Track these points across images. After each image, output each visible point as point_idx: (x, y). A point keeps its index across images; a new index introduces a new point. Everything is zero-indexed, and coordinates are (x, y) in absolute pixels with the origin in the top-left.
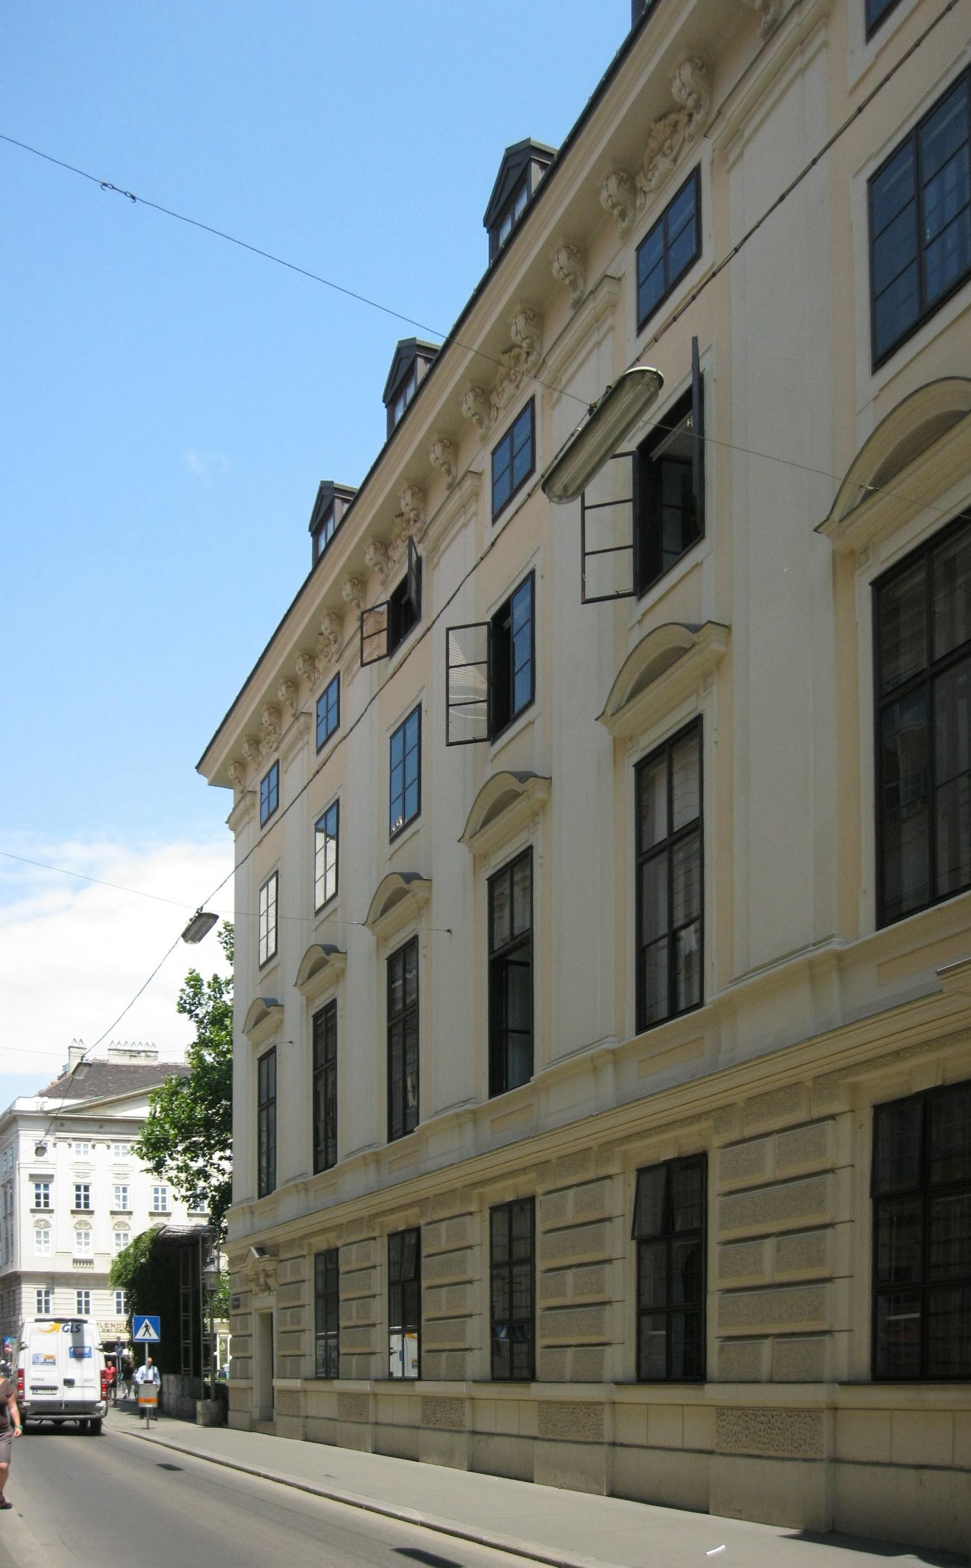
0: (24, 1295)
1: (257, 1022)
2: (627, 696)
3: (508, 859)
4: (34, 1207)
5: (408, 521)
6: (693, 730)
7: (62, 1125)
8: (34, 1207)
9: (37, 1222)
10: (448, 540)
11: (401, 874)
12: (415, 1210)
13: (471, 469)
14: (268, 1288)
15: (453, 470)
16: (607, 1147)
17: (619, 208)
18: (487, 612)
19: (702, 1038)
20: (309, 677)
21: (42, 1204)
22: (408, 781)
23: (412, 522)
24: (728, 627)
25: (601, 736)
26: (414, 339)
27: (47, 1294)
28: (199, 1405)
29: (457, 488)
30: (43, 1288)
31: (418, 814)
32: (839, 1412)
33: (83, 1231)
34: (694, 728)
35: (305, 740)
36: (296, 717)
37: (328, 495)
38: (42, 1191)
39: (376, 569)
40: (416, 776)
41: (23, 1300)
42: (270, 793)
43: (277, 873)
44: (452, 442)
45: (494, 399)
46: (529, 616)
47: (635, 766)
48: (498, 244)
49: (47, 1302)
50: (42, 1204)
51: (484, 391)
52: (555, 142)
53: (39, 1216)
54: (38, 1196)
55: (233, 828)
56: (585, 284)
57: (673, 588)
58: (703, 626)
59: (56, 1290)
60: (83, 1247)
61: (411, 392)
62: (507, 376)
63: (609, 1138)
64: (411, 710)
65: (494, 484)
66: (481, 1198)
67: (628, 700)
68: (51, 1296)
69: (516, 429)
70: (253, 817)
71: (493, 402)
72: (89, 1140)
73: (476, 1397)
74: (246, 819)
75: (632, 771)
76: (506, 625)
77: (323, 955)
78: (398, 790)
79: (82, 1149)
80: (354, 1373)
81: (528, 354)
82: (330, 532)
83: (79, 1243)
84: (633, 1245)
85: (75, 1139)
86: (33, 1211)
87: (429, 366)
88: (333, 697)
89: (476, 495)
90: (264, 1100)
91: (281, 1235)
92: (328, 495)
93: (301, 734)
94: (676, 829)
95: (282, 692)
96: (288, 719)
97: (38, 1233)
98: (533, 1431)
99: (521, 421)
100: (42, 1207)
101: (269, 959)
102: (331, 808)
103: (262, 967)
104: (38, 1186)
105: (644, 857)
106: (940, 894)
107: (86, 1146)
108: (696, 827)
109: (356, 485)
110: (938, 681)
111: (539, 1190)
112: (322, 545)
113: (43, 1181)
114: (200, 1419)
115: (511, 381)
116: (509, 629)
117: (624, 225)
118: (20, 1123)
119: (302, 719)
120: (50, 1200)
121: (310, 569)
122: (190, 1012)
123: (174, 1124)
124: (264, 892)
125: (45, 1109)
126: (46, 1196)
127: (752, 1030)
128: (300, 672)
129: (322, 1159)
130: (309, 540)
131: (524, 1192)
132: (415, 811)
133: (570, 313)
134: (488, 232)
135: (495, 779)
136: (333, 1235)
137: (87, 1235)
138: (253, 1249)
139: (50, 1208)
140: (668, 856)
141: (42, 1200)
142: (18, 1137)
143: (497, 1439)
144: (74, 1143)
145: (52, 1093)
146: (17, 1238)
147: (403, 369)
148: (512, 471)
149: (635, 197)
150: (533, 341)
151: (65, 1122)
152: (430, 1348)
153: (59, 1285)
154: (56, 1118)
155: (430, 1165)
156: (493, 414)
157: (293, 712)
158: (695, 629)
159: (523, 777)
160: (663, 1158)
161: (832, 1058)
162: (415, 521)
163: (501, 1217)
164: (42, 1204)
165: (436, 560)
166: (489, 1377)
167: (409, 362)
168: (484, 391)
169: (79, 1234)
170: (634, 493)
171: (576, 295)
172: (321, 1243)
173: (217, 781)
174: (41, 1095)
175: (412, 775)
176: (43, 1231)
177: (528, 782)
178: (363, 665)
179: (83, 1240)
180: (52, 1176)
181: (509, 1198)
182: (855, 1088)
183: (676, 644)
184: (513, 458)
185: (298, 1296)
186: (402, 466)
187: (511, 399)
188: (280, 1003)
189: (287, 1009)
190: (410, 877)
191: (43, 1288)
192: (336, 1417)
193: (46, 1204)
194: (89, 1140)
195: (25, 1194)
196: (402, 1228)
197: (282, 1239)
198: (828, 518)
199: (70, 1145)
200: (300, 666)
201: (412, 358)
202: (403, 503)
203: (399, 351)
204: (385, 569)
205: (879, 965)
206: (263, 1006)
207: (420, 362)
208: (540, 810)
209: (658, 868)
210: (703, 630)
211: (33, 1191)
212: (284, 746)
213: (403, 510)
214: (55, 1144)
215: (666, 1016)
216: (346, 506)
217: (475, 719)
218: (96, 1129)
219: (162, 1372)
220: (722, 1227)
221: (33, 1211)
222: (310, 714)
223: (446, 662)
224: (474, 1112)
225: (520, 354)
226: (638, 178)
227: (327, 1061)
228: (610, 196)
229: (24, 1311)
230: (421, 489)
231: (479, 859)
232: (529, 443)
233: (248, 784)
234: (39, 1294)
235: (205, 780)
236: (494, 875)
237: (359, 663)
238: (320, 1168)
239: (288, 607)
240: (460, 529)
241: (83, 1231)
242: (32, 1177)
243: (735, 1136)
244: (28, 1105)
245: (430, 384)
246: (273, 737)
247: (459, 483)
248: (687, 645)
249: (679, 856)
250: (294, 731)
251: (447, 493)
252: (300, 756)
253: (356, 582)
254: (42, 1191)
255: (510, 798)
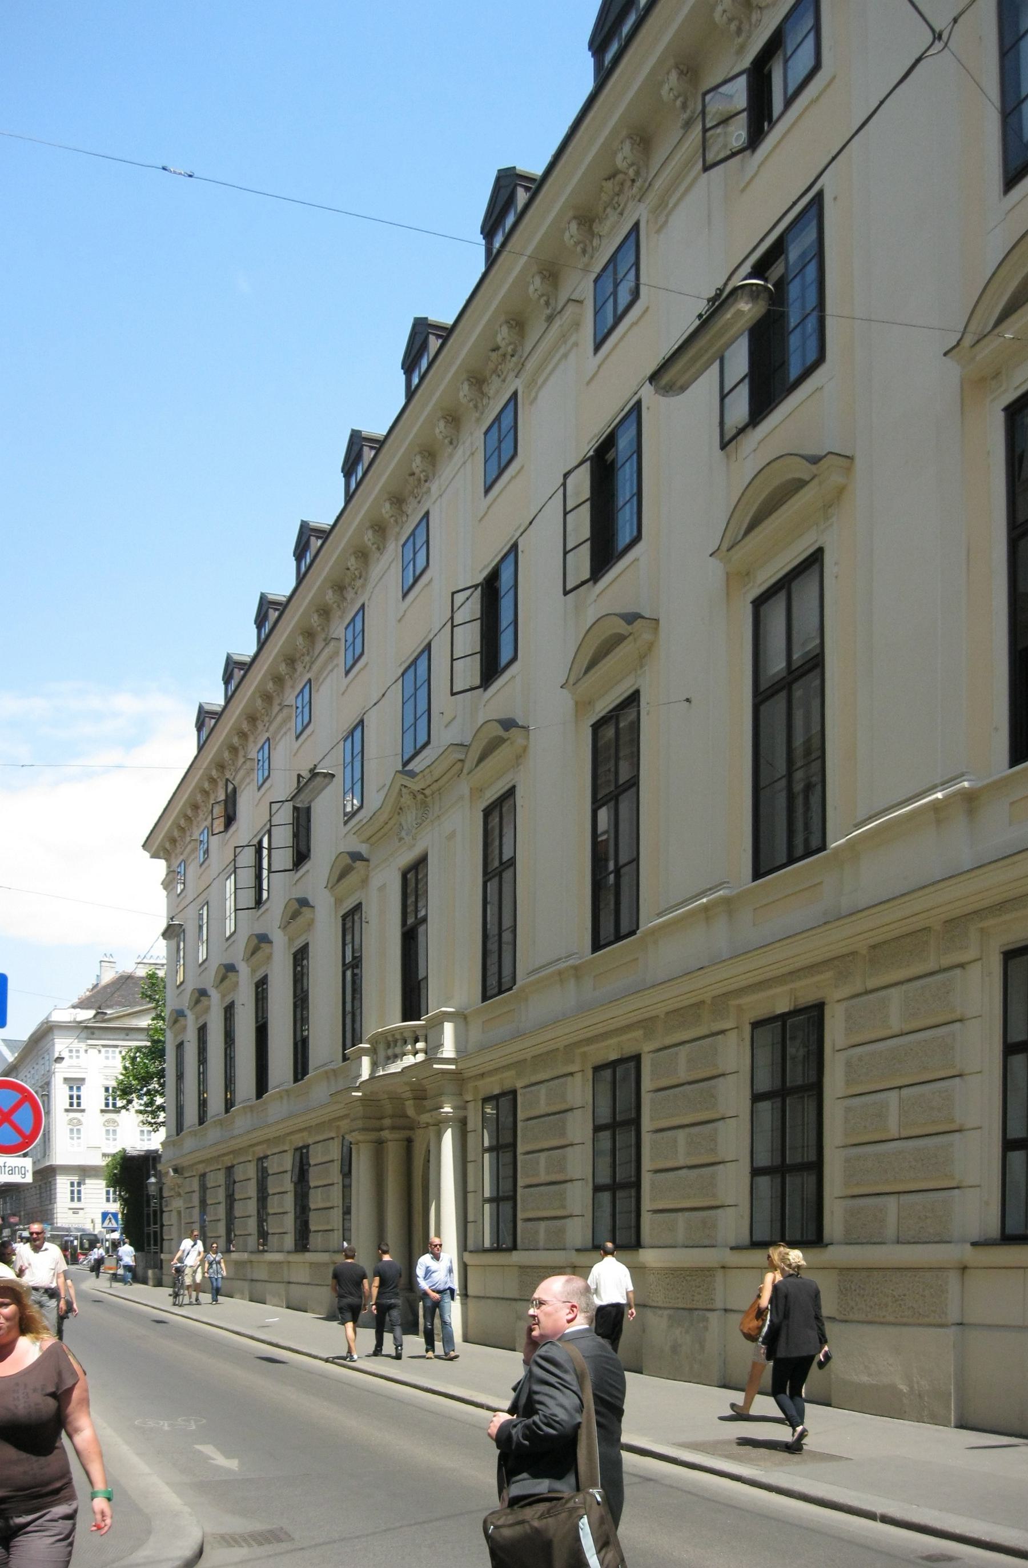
0: (58, 1186)
1: (253, 953)
2: (742, 532)
3: (626, 695)
4: (68, 1107)
5: (504, 355)
6: (814, 560)
7: (93, 1034)
8: (68, 1107)
9: (71, 1120)
10: (545, 375)
11: (348, 853)
12: (512, 1073)
13: (573, 297)
14: (179, 1195)
15: (552, 302)
16: (570, 1048)
17: (635, 167)
18: (480, 572)
19: (637, 959)
20: (476, 407)
21: (75, 1104)
22: (355, 780)
23: (509, 357)
24: (850, 458)
25: (715, 570)
26: (514, 168)
27: (79, 1184)
28: (150, 1272)
29: (558, 316)
30: (75, 1179)
31: (428, 743)
32: (968, 1271)
33: (111, 1128)
34: (815, 559)
35: (335, 662)
36: (327, 641)
37: (307, 534)
38: (75, 1093)
39: (446, 441)
40: (426, 707)
41: (58, 1190)
42: (354, 638)
43: (207, 903)
44: (551, 274)
45: (597, 228)
46: (635, 448)
47: (592, 726)
48: (603, 61)
49: (79, 1192)
50: (75, 1104)
51: (587, 220)
52: (537, 169)
53: (72, 1115)
54: (71, 1097)
55: (165, 888)
56: (647, 173)
57: (619, 575)
58: (825, 456)
59: (87, 1181)
60: (111, 1142)
61: (424, 364)
62: (494, 371)
63: (571, 1041)
64: (419, 650)
65: (596, 313)
66: (254, 1152)
67: (477, 766)
68: (83, 1187)
69: (620, 256)
70: (337, 665)
71: (596, 230)
72: (116, 1046)
73: (728, 1265)
74: (284, 730)
75: (590, 730)
76: (610, 457)
77: (349, 861)
78: (409, 720)
79: (110, 1055)
80: (891, 1232)
81: (633, 181)
82: (360, 474)
83: (108, 1139)
84: (341, 1177)
85: (104, 1046)
86: (67, 1110)
87: (440, 341)
88: (420, 540)
89: (577, 325)
90: (349, 959)
91: (184, 1162)
92: (357, 442)
93: (331, 658)
94: (762, 689)
95: (315, 620)
96: (320, 644)
97: (72, 1130)
98: (307, 1281)
99: (506, 412)
100: (75, 1107)
101: (232, 935)
102: (422, 652)
103: (178, 987)
104: (71, 1088)
105: (761, 697)
106: (602, 943)
107: (114, 1052)
108: (816, 663)
109: (449, 320)
110: (795, 686)
111: (519, 1084)
112: (353, 485)
113: (75, 1084)
114: (151, 1282)
115: (615, 209)
116: (613, 462)
117: (741, 40)
118: (56, 1032)
119: (333, 643)
120: (82, 1101)
121: (482, 269)
122: (150, 997)
123: (136, 1078)
124: (228, 882)
125: (78, 1019)
126: (79, 1097)
127: (874, 878)
128: (387, 516)
129: (493, 981)
130: (342, 480)
131: (629, 1050)
132: (426, 739)
133: (681, 132)
134: (593, 55)
135: (772, 465)
136: (305, 1134)
137: (114, 1131)
138: (171, 1170)
139: (82, 1107)
140: (788, 693)
141: (75, 1101)
142: (53, 1045)
143: (259, 1283)
144: (103, 1050)
145: (82, 1005)
146: (52, 1134)
147: (417, 345)
148: (500, 453)
149: (751, 12)
150: (586, 245)
151: (96, 1031)
152: (531, 1215)
153: (90, 1177)
154: (86, 1027)
155: (236, 1132)
156: (754, 17)
157: (323, 636)
158: (815, 460)
159: (631, 618)
160: (779, 1012)
161: (866, 935)
162: (512, 356)
163: (766, 1035)
164: (75, 1104)
165: (533, 394)
166: (590, 1245)
167: (509, 190)
168: (587, 220)
169: (108, 1131)
170: (482, 614)
171: (549, 312)
172: (298, 1141)
173: (155, 856)
174: (74, 1007)
175: (422, 706)
176: (75, 1128)
177: (635, 624)
178: (706, 168)
179: (111, 1136)
180: (83, 1080)
181: (613, 1056)
182: (584, 1055)
183: (797, 475)
184: (500, 442)
185: (562, 1132)
186: (499, 297)
187: (497, 392)
188: (311, 903)
189: (318, 908)
190: (508, 724)
191: (75, 1179)
192: (267, 1279)
193: (79, 1104)
194: (116, 1046)
195: (60, 1095)
196: (496, 1092)
197: (185, 1164)
198: (958, 344)
199: (100, 1051)
200: (386, 509)
201: (511, 187)
202: (414, 465)
203: (498, 179)
204: (480, 405)
205: (1012, 804)
206: (296, 906)
207: (432, 339)
208: (643, 657)
209: (778, 705)
210: (822, 462)
211: (67, 1093)
212: (316, 667)
213: (619, 167)
214: (86, 1051)
215: (785, 861)
216: (373, 452)
217: (469, 671)
218: (122, 1036)
219: (136, 1250)
220: (652, 1119)
221: (67, 1110)
222: (338, 639)
223: (540, 502)
224: (576, 968)
225: (625, 180)
226: (594, 226)
227: (354, 958)
228: (724, 11)
229: (58, 1200)
230: (518, 324)
231: (581, 706)
232: (512, 431)
233: (331, 631)
234: (72, 1185)
235: (147, 855)
236: (488, 807)
237: (699, 165)
238: (489, 994)
239: (467, 296)
240: (560, 360)
241: (111, 1128)
242: (66, 1080)
243: (859, 988)
244: (64, 1015)
245: (256, 663)
246: (307, 659)
247: (560, 312)
248: (626, 634)
249: (798, 693)
250: (279, 719)
251: (545, 325)
252: (329, 679)
253: (427, 454)
254: (75, 1093)
255: (617, 640)
